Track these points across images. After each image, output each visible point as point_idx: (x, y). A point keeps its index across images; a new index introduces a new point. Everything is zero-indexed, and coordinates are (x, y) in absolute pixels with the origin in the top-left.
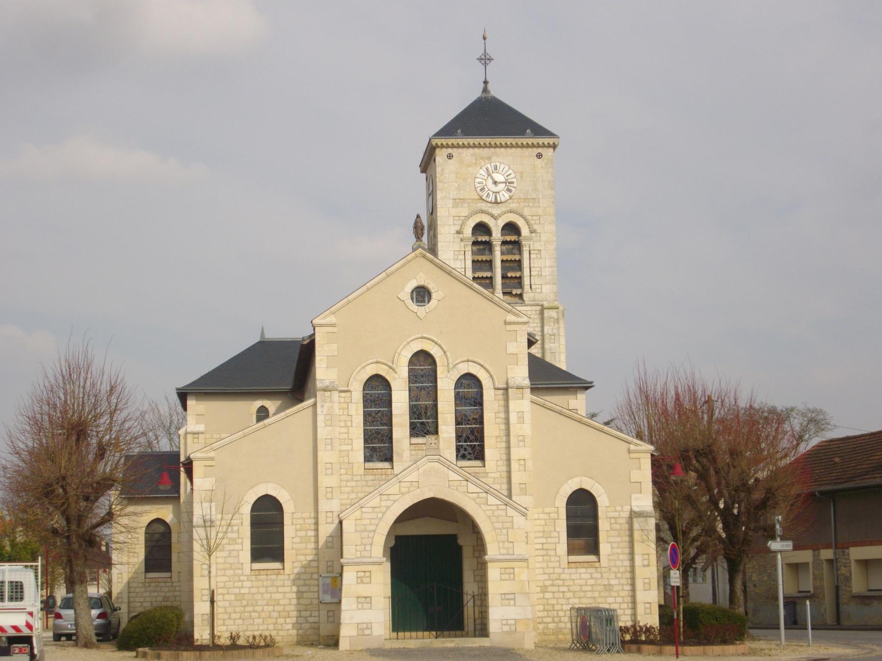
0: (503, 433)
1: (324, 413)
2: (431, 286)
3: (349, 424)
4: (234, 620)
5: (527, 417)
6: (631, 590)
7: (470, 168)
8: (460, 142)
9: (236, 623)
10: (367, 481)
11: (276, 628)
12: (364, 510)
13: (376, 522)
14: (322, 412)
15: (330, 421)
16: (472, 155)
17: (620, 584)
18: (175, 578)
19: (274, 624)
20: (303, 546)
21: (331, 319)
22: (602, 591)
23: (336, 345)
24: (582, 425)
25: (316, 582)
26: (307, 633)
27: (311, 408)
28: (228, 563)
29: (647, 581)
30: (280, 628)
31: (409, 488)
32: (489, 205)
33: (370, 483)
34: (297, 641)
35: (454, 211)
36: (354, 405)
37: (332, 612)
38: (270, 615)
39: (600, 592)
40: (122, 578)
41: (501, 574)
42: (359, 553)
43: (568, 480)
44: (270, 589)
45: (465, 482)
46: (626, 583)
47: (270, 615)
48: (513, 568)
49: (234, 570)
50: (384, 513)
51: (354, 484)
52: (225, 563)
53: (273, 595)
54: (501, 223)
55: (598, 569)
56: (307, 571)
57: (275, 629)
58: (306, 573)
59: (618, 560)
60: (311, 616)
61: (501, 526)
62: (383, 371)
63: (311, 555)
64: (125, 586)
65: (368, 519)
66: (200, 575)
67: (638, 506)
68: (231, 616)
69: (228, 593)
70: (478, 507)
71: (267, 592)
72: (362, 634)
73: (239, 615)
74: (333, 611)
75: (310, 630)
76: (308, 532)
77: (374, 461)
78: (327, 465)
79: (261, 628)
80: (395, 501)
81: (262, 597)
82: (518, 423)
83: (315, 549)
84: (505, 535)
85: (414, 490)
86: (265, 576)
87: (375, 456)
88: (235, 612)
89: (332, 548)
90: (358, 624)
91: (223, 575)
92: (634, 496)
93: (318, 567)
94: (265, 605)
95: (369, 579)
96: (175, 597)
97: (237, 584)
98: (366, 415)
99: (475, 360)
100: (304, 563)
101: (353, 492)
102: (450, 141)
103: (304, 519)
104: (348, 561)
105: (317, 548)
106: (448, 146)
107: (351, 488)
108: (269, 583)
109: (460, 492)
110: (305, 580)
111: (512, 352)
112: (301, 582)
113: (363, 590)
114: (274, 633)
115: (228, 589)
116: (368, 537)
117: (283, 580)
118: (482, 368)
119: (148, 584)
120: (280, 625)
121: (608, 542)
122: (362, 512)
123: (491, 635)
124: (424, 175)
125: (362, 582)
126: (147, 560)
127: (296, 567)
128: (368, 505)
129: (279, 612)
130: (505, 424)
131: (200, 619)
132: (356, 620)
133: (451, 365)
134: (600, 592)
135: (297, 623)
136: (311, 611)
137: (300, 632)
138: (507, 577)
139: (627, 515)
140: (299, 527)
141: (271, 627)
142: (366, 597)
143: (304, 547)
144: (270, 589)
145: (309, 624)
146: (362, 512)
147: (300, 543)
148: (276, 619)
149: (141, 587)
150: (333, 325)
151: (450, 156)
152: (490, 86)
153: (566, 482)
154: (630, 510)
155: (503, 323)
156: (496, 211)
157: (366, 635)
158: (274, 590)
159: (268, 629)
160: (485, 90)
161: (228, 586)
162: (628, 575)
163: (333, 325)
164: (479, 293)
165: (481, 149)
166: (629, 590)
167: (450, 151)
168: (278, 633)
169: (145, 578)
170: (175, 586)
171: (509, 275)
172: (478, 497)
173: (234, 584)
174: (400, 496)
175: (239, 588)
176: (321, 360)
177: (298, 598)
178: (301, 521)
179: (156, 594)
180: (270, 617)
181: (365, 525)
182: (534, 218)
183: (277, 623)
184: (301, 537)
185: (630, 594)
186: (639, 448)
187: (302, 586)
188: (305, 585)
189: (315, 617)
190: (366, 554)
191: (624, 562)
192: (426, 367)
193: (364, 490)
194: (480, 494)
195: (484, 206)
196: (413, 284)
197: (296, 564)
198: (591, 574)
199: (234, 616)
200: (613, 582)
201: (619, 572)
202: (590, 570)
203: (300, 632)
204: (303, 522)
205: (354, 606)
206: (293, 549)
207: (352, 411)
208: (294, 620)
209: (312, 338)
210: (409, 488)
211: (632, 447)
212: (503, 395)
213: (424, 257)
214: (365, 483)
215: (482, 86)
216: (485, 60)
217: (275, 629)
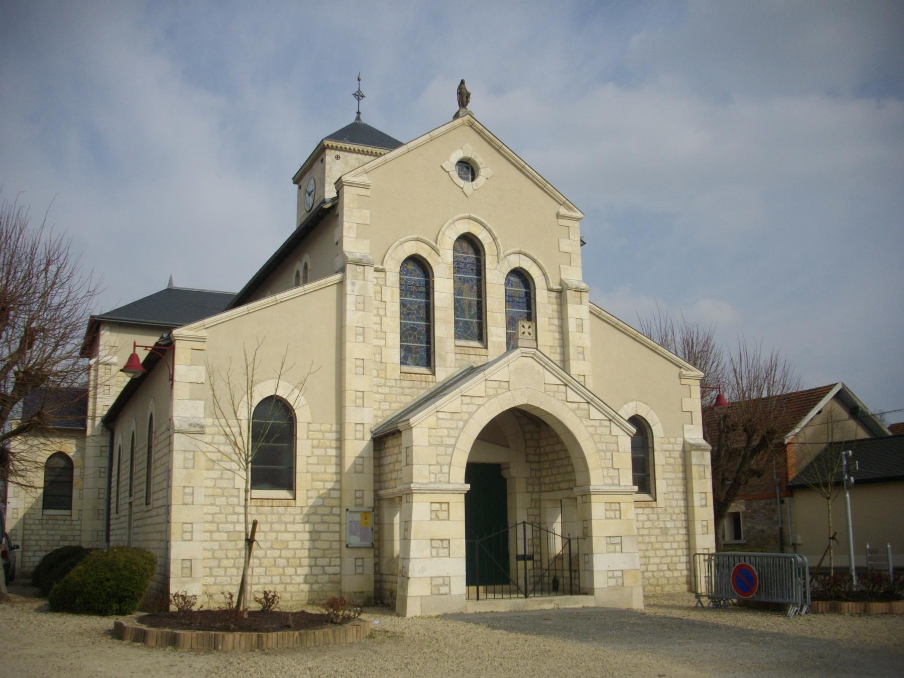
0: (557, 343)
1: (355, 293)
2: (479, 160)
3: (382, 312)
4: (226, 568)
5: (587, 324)
6: (686, 534)
8: (348, 146)
9: (228, 574)
10: (403, 388)
11: (283, 581)
12: (440, 415)
13: (454, 433)
14: (353, 291)
15: (362, 305)
16: (356, 159)
17: (675, 527)
18: (75, 516)
19: (281, 575)
20: (321, 468)
21: (363, 179)
22: (659, 535)
23: (369, 211)
24: (636, 342)
25: (337, 519)
26: (324, 588)
27: (335, 287)
28: (218, 488)
29: (705, 523)
30: (289, 581)
31: (496, 389)
33: (407, 391)
34: (309, 600)
36: (389, 289)
37: (361, 560)
38: (275, 562)
39: (657, 536)
40: (17, 513)
41: (606, 510)
42: (433, 476)
44: (276, 527)
45: (563, 387)
46: (681, 526)
47: (275, 562)
48: (619, 503)
49: (227, 497)
50: (466, 422)
51: (387, 390)
52: (215, 486)
53: (280, 534)
55: (655, 509)
56: (326, 504)
57: (281, 583)
58: (326, 506)
59: (673, 499)
60: (330, 565)
61: (604, 448)
62: (424, 252)
63: (332, 481)
64: (18, 522)
65: (446, 428)
66: (181, 503)
67: (691, 439)
68: (221, 564)
69: (218, 531)
70: (579, 421)
71: (271, 531)
72: (437, 592)
73: (232, 561)
74: (363, 558)
75: (328, 584)
76: (328, 450)
77: (409, 365)
78: (357, 361)
79: (262, 580)
81: (265, 536)
82: (577, 332)
83: (336, 473)
84: (609, 459)
85: (503, 393)
86: (269, 508)
87: (410, 358)
88: (227, 558)
89: (362, 472)
90: (432, 578)
91: (212, 505)
92: (687, 427)
93: (340, 498)
94: (268, 549)
95: (446, 513)
96: (74, 536)
97: (230, 518)
98: (403, 304)
99: (528, 252)
100: (322, 492)
101: (385, 401)
102: (340, 145)
103: (323, 432)
104: (422, 486)
105: (340, 473)
106: (336, 149)
107: (383, 396)
108: (274, 518)
109: (558, 399)
110: (323, 515)
112: (317, 518)
113: (441, 529)
114: (280, 588)
115: (218, 524)
116: (446, 454)
117: (294, 515)
118: (534, 264)
119: (45, 521)
120: (289, 577)
121: (664, 479)
122: (438, 419)
123: (596, 592)
124: (296, 186)
125: (438, 518)
126: (45, 494)
127: (311, 498)
128: (445, 409)
129: (288, 559)
130: (559, 332)
131: (179, 566)
132: (428, 574)
133: (502, 255)
134: (657, 536)
135: (312, 574)
136: (330, 558)
137: (315, 586)
138: (611, 514)
139: (679, 448)
140: (315, 442)
141: (276, 579)
142: (442, 540)
143: (323, 470)
144: (276, 527)
145: (327, 576)
146: (438, 419)
147: (317, 464)
148: (284, 568)
149: (38, 524)
150: (366, 187)
151: (338, 157)
152: (361, 116)
154: (682, 443)
155: (555, 216)
157: (443, 594)
158: (281, 527)
159: (272, 583)
160: (358, 118)
161: (218, 520)
162: (683, 517)
163: (366, 187)
164: (529, 177)
165: (363, 156)
166: (683, 534)
167: (337, 153)
168: (285, 589)
169: (43, 515)
170: (75, 525)
172: (578, 408)
173: (226, 517)
174: (485, 399)
175: (234, 523)
176: (350, 227)
177: (312, 540)
178: (319, 435)
179: (53, 532)
180: (275, 565)
181: (441, 437)
183: (284, 574)
184: (318, 456)
185: (685, 539)
187: (319, 523)
188: (323, 522)
189: (335, 566)
190: (443, 478)
191: (678, 501)
193: (399, 400)
194: (580, 404)
196: (458, 155)
197: (311, 494)
198: (648, 514)
199: (225, 563)
200: (669, 525)
201: (674, 513)
202: (647, 511)
203: (315, 586)
204: (321, 437)
205: (427, 552)
206: (308, 472)
207: (387, 297)
208: (306, 570)
209: (336, 202)
210: (496, 389)
211: (685, 372)
212: (556, 298)
213: (471, 126)
214: (400, 391)
215: (356, 115)
216: (359, 96)
217: (281, 583)
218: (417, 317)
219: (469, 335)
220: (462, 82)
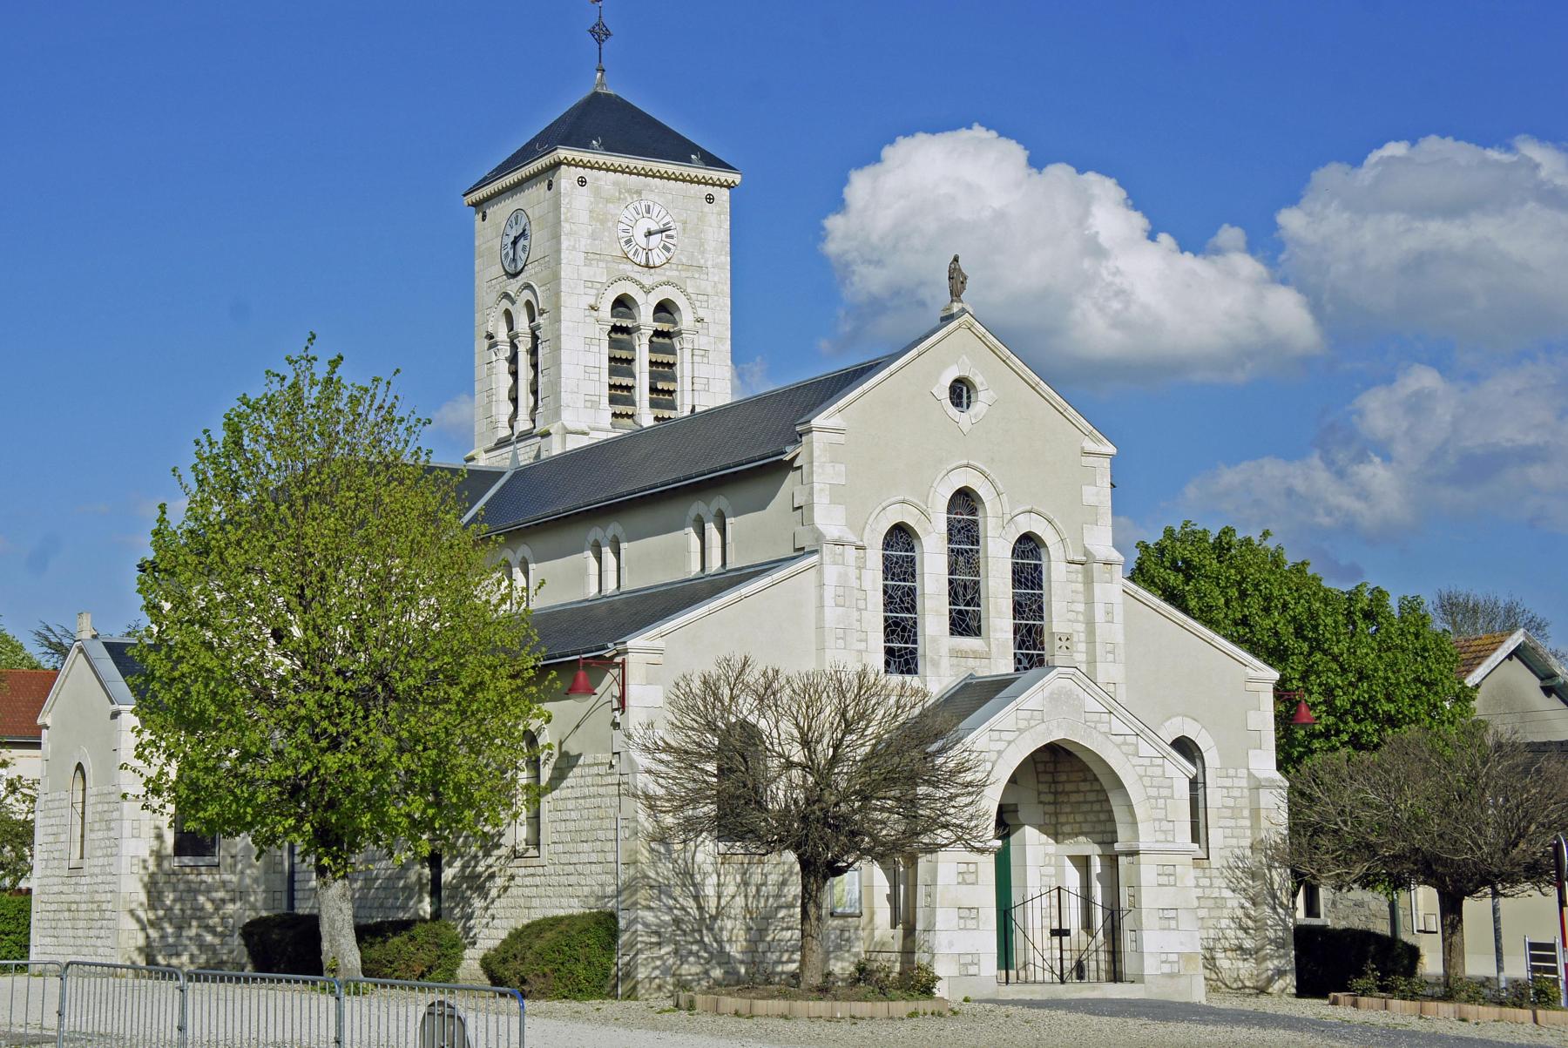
2: (978, 380)
5: (1119, 617)
7: (610, 205)
31: (1028, 720)
32: (637, 268)
35: (587, 273)
43: (1165, 721)
54: (654, 299)
55: (1207, 871)
80: (1009, 743)
99: (1041, 510)
111: (1090, 503)
113: (968, 896)
138: (1164, 880)
142: (969, 909)
151: (582, 182)
153: (1203, 727)
156: (648, 279)
171: (660, 386)
172: (1125, 743)
176: (822, 490)
182: (700, 297)
186: (1260, 674)
192: (965, 517)
195: (628, 268)
207: (867, 585)
218: (901, 608)
219: (964, 630)
220: (956, 259)
